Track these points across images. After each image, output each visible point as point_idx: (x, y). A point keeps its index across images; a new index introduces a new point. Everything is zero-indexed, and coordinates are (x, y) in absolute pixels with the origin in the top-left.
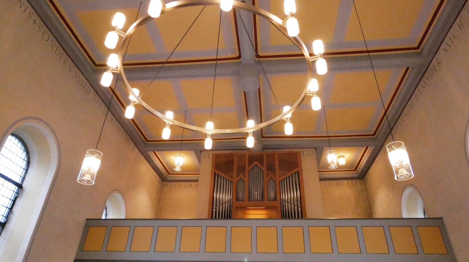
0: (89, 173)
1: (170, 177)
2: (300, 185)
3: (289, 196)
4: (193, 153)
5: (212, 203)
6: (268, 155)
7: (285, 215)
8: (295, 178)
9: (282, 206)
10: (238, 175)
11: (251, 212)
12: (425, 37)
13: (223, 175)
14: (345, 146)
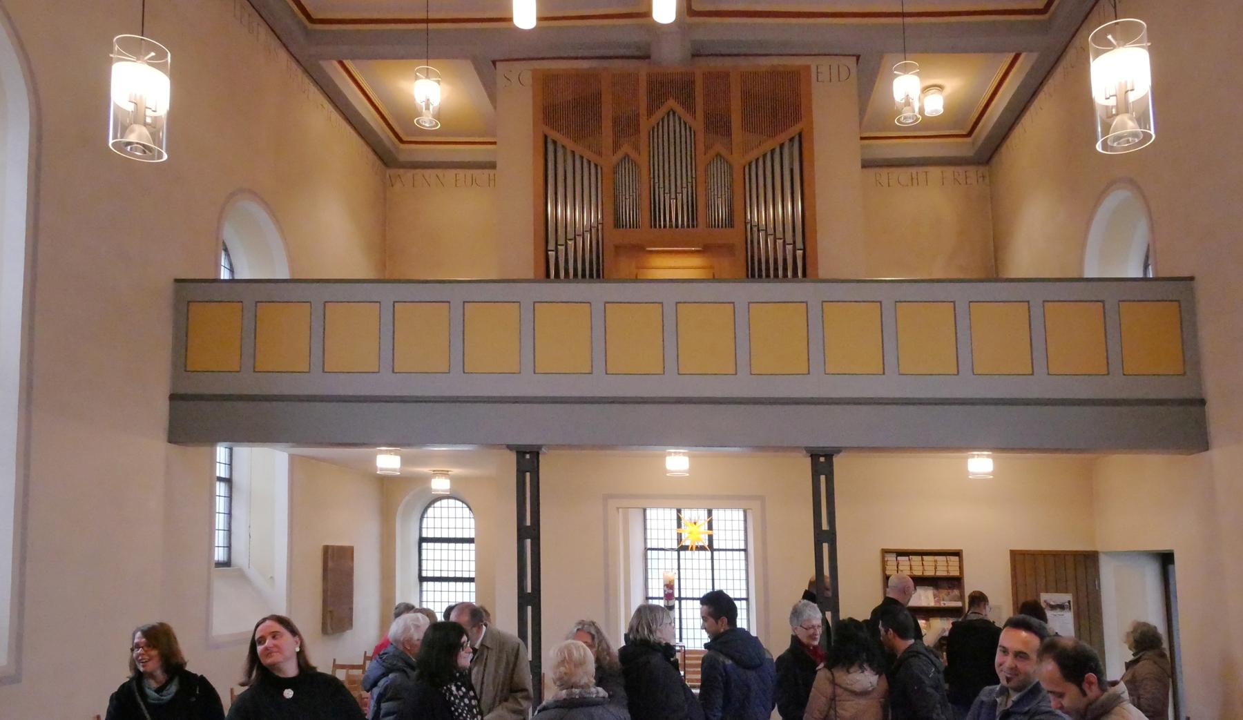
0: (138, 117)
1: (407, 153)
2: (802, 182)
3: (770, 213)
4: (468, 66)
5: (542, 233)
6: (709, 76)
7: (756, 270)
8: (790, 156)
9: (749, 245)
10: (616, 147)
11: (658, 261)
13: (570, 145)
14: (953, 50)
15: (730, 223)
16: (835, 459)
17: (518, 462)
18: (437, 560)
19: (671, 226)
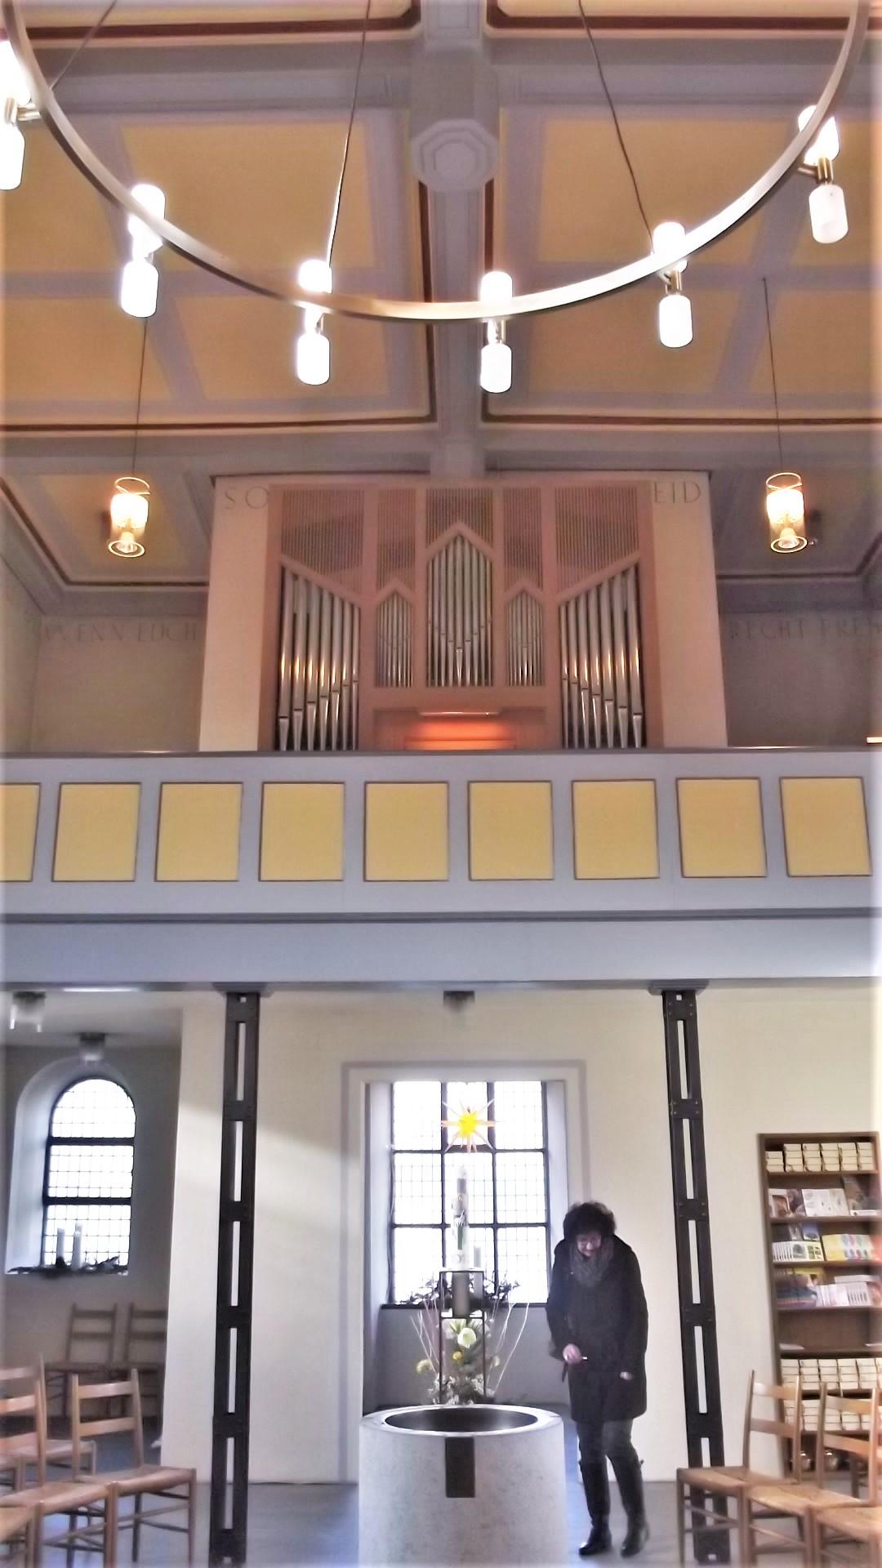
9: (567, 708)
10: (381, 582)
15: (538, 678)
16: (698, 998)
17: (229, 1009)
18: (72, 1171)
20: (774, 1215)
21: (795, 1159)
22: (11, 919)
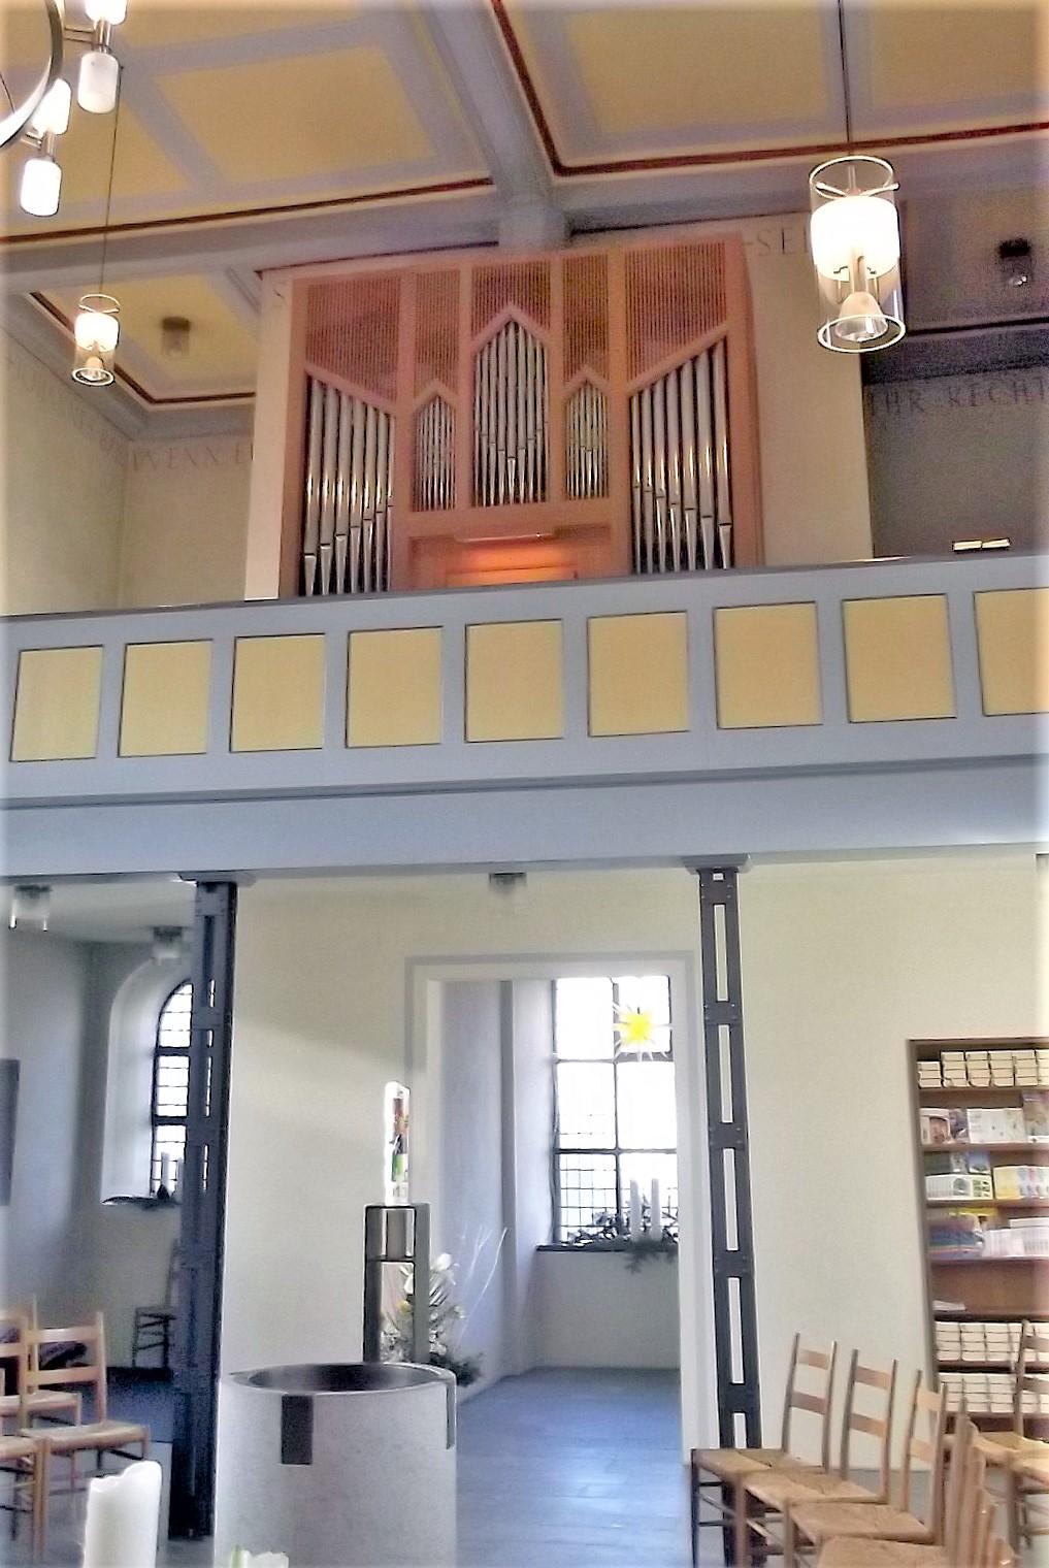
3: (682, 472)
6: (422, 281)
12: (548, 150)
19: (517, 500)
20: (928, 1141)
21: (954, 1071)
22: (14, 805)
